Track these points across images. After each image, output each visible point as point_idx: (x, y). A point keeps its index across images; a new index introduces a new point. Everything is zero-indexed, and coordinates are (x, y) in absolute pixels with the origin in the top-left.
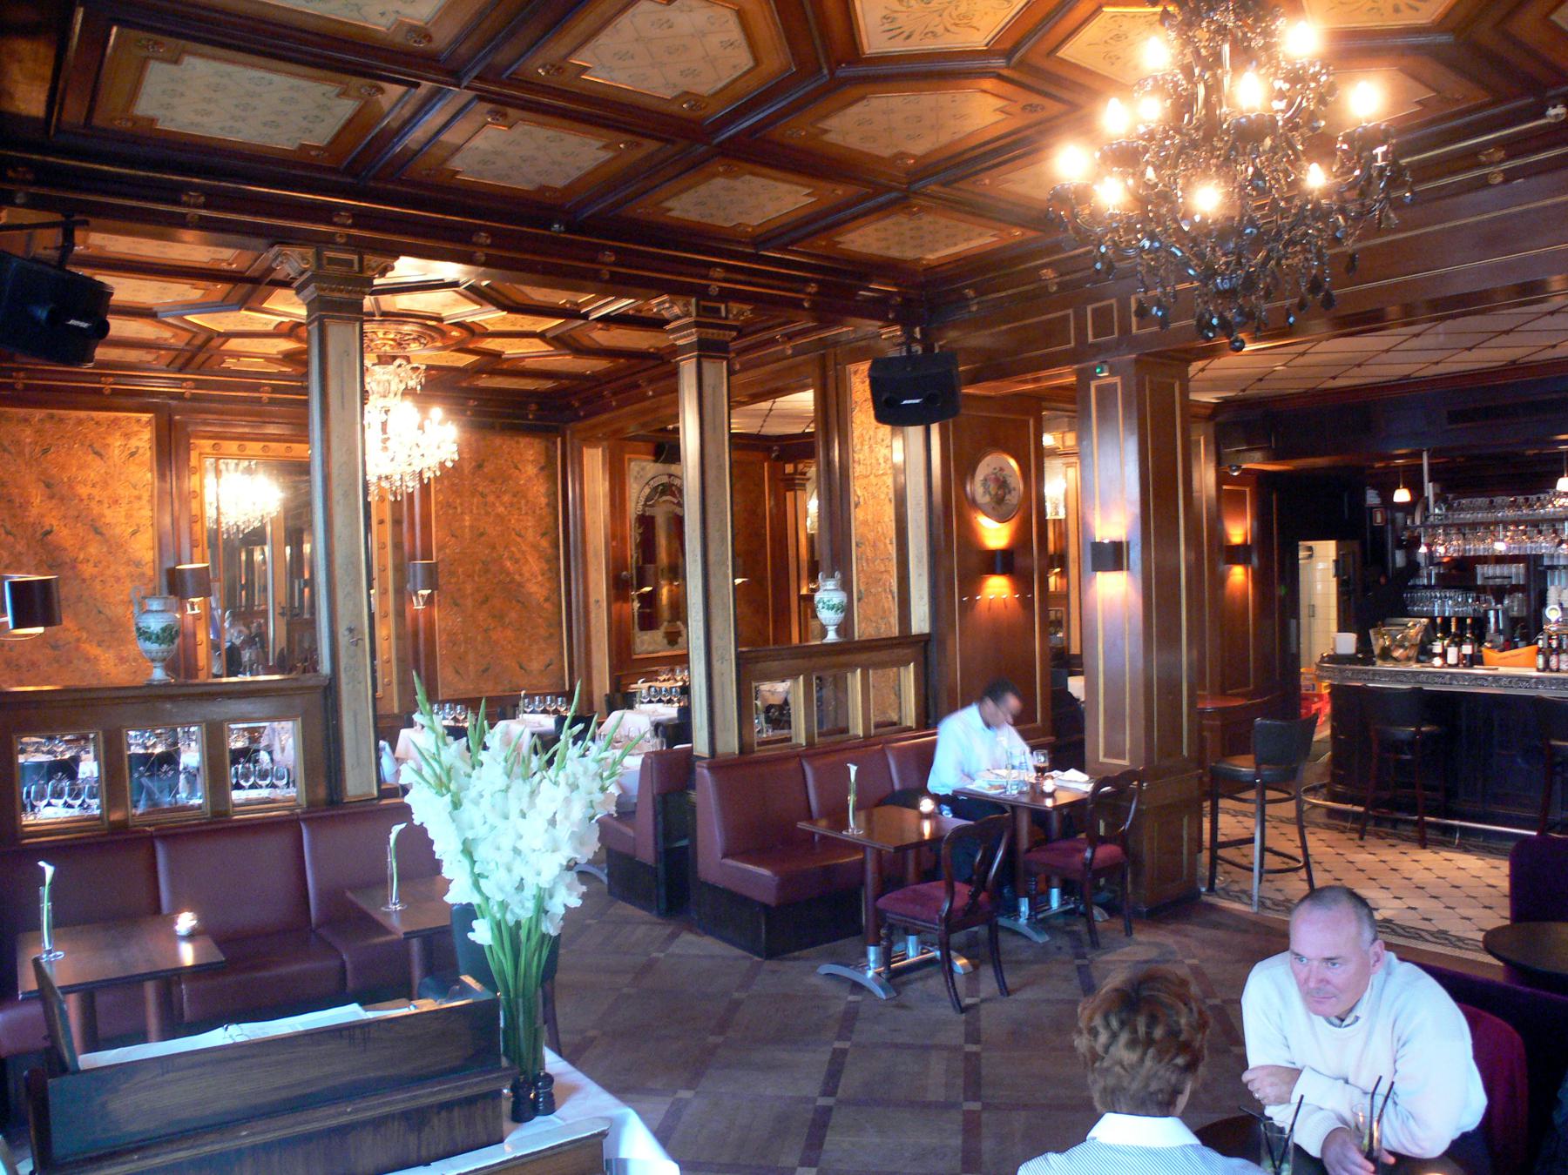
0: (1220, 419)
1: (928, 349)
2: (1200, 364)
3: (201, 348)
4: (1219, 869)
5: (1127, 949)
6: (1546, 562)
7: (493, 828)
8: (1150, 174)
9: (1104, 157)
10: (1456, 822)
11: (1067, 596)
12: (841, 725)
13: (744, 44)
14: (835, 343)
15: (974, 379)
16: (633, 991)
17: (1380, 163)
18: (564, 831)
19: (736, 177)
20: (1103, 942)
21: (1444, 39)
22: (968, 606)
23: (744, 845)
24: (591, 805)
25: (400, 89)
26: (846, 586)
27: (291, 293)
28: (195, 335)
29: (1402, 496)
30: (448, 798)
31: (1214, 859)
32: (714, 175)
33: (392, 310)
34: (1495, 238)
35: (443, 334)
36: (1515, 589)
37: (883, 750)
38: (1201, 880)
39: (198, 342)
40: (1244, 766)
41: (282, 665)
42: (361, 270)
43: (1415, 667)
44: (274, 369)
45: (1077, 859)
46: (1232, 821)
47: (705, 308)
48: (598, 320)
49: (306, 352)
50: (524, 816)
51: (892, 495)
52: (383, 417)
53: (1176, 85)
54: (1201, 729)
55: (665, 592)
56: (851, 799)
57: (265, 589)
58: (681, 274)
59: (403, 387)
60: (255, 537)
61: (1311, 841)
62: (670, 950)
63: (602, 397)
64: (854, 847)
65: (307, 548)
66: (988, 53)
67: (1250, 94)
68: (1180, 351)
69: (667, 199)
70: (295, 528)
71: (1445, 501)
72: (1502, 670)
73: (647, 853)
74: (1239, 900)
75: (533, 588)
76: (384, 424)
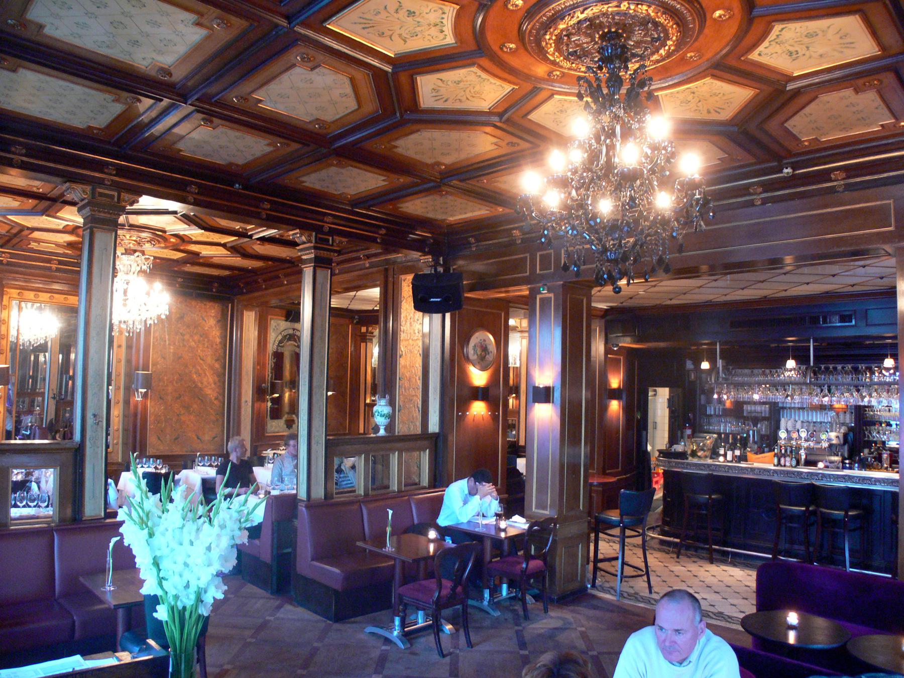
0: (608, 318)
1: (447, 270)
2: (599, 288)
3: (15, 235)
4: (598, 573)
5: (545, 621)
6: (780, 405)
7: (173, 550)
8: (574, 193)
9: (549, 182)
10: (729, 549)
13: (353, 95)
14: (394, 262)
15: (472, 289)
17: (697, 196)
18: (215, 554)
22: (461, 418)
23: (323, 554)
24: (233, 538)
25: (151, 101)
26: (392, 403)
27: (75, 209)
28: (12, 227)
29: (705, 365)
30: (146, 531)
31: (596, 569)
32: (332, 165)
33: (136, 223)
34: (756, 233)
35: (165, 240)
36: (764, 419)
37: (409, 500)
38: (588, 581)
39: (14, 231)
40: (614, 516)
41: (50, 430)
43: (709, 461)
44: (61, 251)
45: (518, 567)
46: (607, 547)
47: (320, 239)
48: (258, 239)
49: (82, 243)
50: (192, 543)
52: (125, 286)
53: (590, 146)
56: (389, 529)
57: (44, 379)
59: (139, 269)
60: (42, 348)
61: (651, 560)
64: (387, 557)
65: (73, 356)
66: (490, 113)
67: (629, 155)
69: (304, 175)
70: (66, 345)
71: (728, 370)
72: (756, 465)
75: (208, 391)
76: (125, 292)
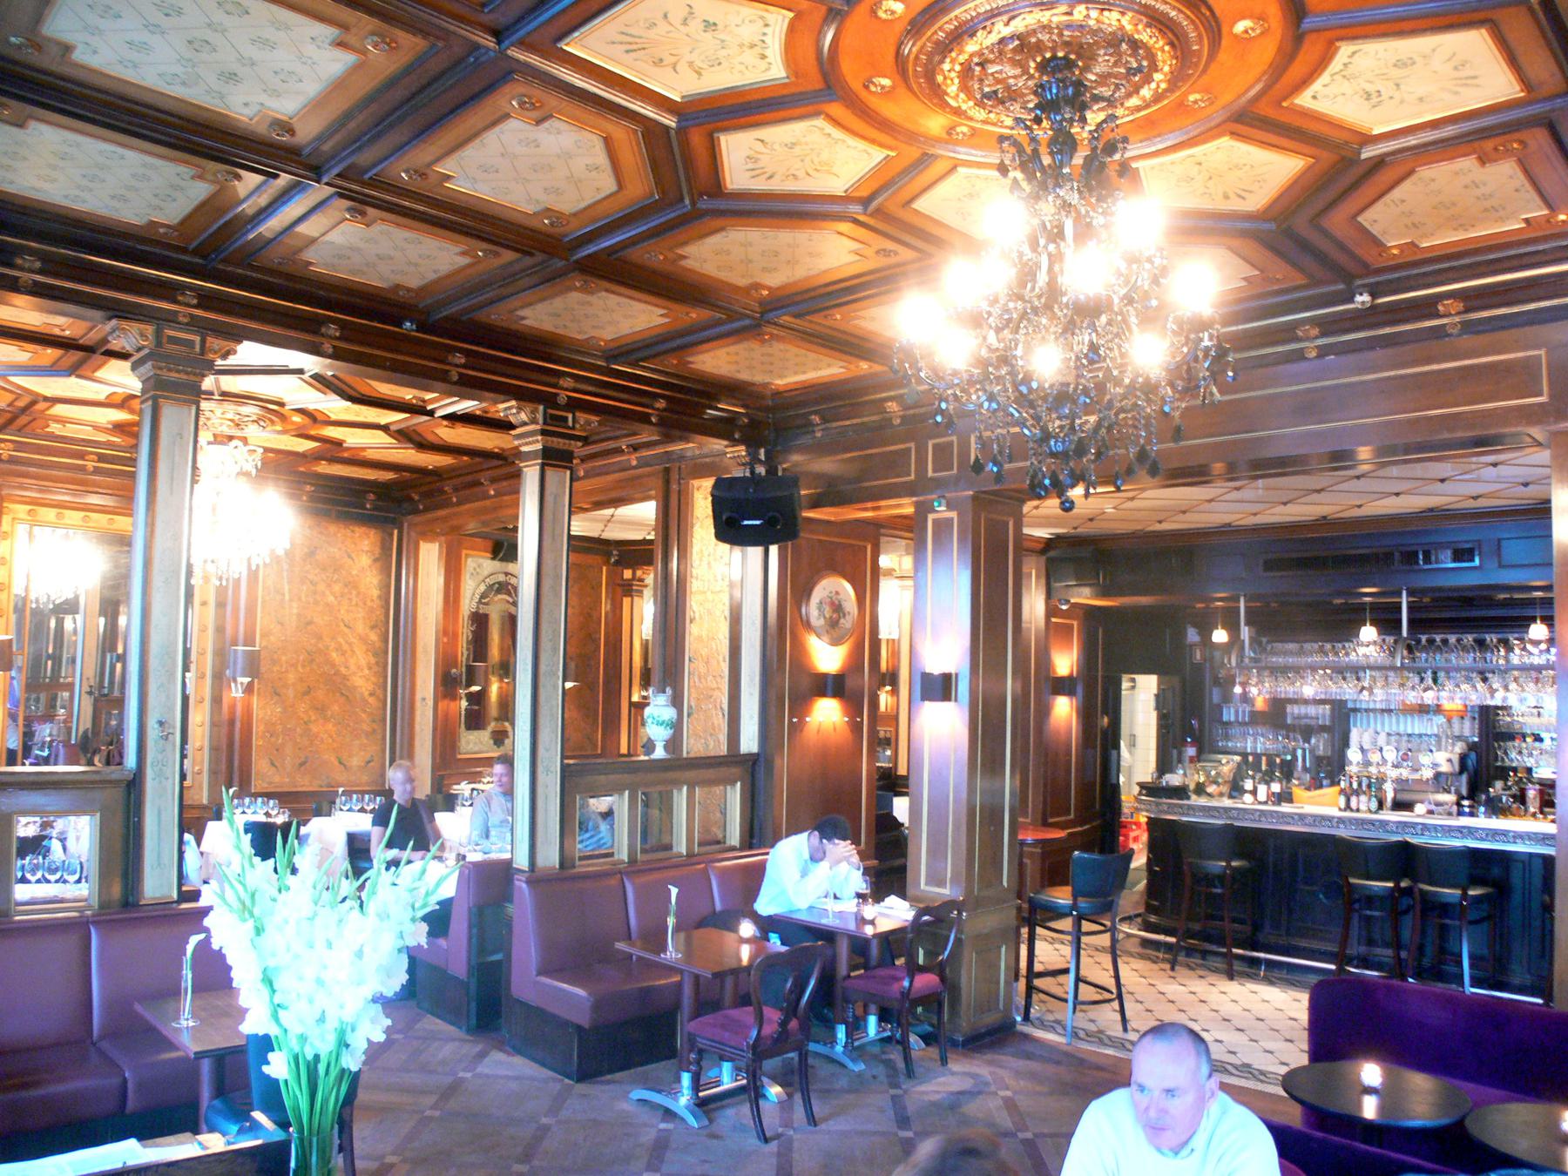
0: (1052, 554)
1: (772, 471)
2: (1035, 503)
3: (24, 410)
6: (1350, 705)
8: (992, 338)
10: (1262, 955)
11: (896, 718)
12: (666, 840)
14: (682, 458)
15: (816, 504)
16: (437, 1113)
19: (592, 293)
20: (918, 1070)
21: (1267, 226)
25: (258, 178)
26: (677, 702)
28: (18, 397)
29: (1220, 636)
30: (250, 924)
31: (1030, 989)
34: (1309, 407)
36: (1323, 728)
38: (1017, 1009)
39: (21, 404)
40: (1062, 897)
41: (84, 749)
42: (203, 352)
43: (1227, 803)
44: (102, 437)
46: (1050, 951)
48: (444, 417)
50: (330, 945)
51: (727, 613)
53: (1021, 254)
54: (1021, 855)
55: (494, 689)
56: (671, 921)
57: (74, 661)
58: (531, 381)
62: (479, 1070)
63: (441, 491)
64: (670, 969)
65: (122, 621)
66: (846, 199)
67: (1087, 272)
68: (1016, 491)
69: (522, 307)
73: (459, 967)
74: (1052, 1029)
